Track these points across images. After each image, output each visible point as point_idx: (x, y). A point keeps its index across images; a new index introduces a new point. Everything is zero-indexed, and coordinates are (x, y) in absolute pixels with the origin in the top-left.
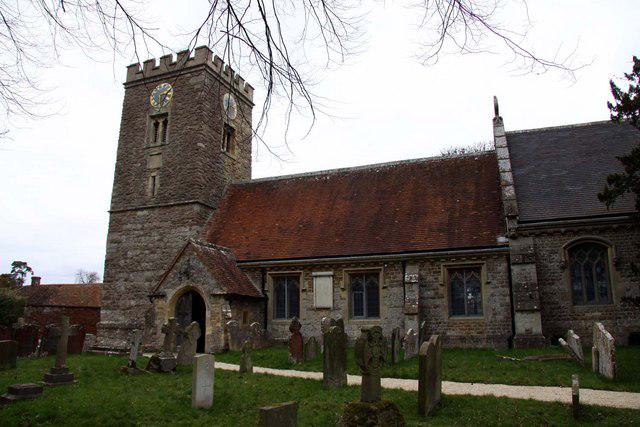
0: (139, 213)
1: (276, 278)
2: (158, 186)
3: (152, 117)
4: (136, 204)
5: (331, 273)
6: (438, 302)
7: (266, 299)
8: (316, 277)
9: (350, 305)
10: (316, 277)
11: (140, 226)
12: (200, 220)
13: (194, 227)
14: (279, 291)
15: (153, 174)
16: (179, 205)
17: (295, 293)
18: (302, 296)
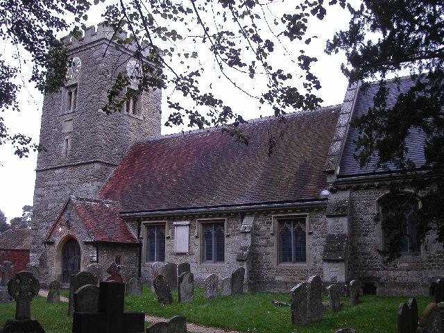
0: (57, 171)
1: (149, 227)
2: (70, 147)
4: (54, 164)
5: (188, 223)
7: (140, 245)
8: (177, 226)
9: (202, 251)
10: (177, 226)
11: (57, 183)
12: (100, 176)
13: (95, 183)
14: (151, 237)
15: (66, 138)
16: (84, 164)
17: (162, 239)
18: (167, 242)
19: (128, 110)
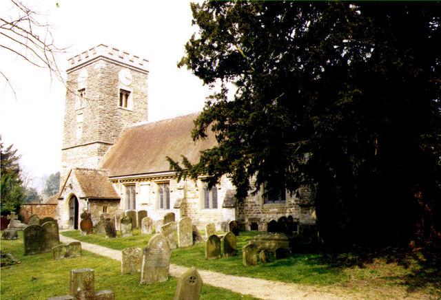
3: (79, 91)
6: (195, 200)
19: (121, 105)
